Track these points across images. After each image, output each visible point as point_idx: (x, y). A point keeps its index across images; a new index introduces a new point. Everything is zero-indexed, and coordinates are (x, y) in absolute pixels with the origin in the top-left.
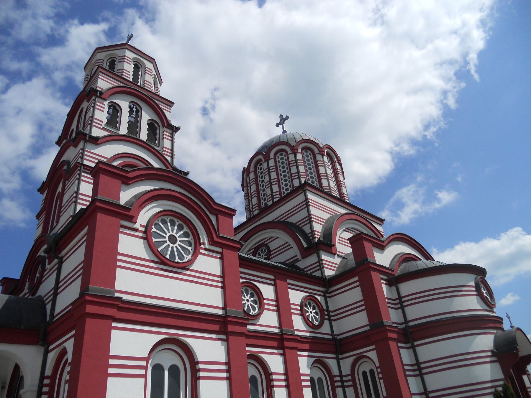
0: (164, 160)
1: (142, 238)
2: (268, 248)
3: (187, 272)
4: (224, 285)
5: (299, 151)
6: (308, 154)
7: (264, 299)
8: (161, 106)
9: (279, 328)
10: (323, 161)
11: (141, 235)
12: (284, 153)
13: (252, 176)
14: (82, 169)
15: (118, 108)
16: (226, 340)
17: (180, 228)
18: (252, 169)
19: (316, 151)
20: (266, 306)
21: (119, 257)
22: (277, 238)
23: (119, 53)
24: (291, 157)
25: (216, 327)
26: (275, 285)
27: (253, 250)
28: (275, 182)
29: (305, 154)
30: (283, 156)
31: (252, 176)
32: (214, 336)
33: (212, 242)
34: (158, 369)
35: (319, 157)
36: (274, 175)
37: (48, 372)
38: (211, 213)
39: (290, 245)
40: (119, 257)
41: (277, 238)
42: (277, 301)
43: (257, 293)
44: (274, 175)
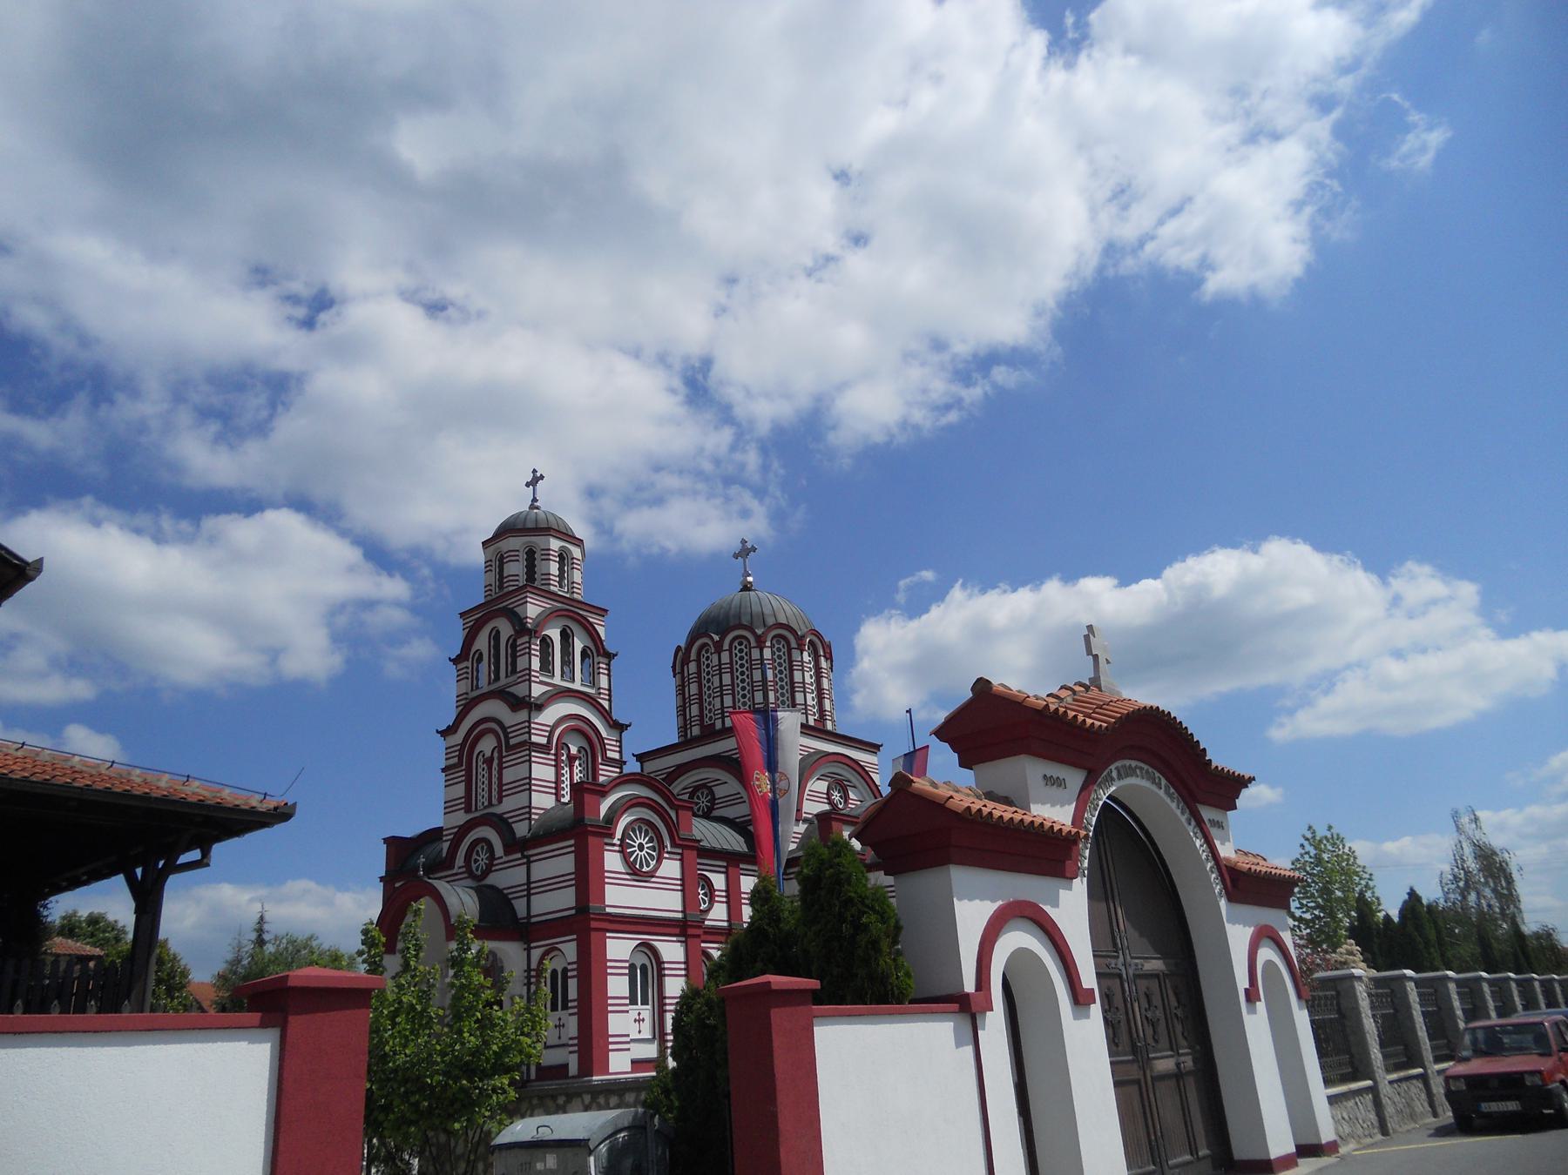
0: (597, 706)
1: (619, 851)
2: (712, 793)
3: (653, 879)
4: (683, 882)
5: (768, 644)
6: (781, 646)
7: (715, 891)
8: (591, 620)
9: (727, 921)
10: (802, 661)
11: (617, 848)
12: (745, 643)
13: (693, 667)
14: (532, 748)
15: (548, 640)
16: (685, 942)
17: (651, 840)
18: (693, 656)
19: (794, 644)
20: (717, 899)
21: (606, 874)
22: (726, 783)
23: (538, 541)
24: (755, 654)
25: (677, 931)
26: (726, 873)
27: (690, 790)
28: (727, 690)
29: (777, 646)
30: (743, 647)
31: (693, 667)
32: (674, 939)
33: (674, 844)
34: (632, 967)
35: (796, 654)
36: (727, 679)
37: (534, 966)
38: (671, 808)
39: (742, 798)
40: (606, 874)
41: (726, 783)
42: (727, 891)
43: (708, 883)
44: (727, 679)
